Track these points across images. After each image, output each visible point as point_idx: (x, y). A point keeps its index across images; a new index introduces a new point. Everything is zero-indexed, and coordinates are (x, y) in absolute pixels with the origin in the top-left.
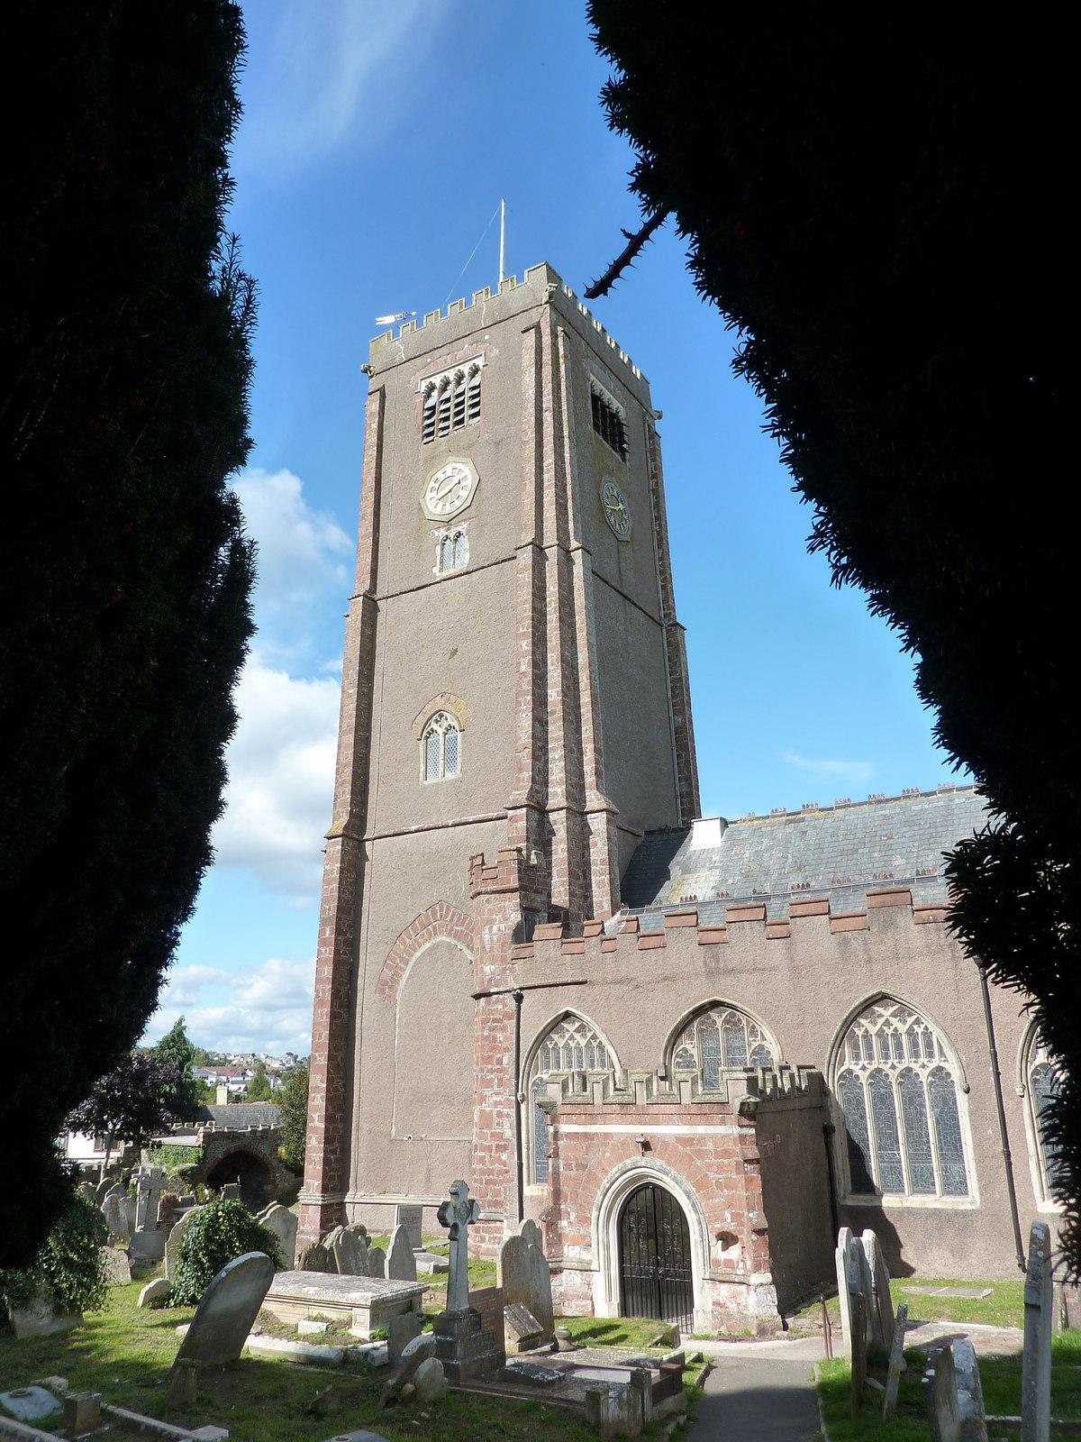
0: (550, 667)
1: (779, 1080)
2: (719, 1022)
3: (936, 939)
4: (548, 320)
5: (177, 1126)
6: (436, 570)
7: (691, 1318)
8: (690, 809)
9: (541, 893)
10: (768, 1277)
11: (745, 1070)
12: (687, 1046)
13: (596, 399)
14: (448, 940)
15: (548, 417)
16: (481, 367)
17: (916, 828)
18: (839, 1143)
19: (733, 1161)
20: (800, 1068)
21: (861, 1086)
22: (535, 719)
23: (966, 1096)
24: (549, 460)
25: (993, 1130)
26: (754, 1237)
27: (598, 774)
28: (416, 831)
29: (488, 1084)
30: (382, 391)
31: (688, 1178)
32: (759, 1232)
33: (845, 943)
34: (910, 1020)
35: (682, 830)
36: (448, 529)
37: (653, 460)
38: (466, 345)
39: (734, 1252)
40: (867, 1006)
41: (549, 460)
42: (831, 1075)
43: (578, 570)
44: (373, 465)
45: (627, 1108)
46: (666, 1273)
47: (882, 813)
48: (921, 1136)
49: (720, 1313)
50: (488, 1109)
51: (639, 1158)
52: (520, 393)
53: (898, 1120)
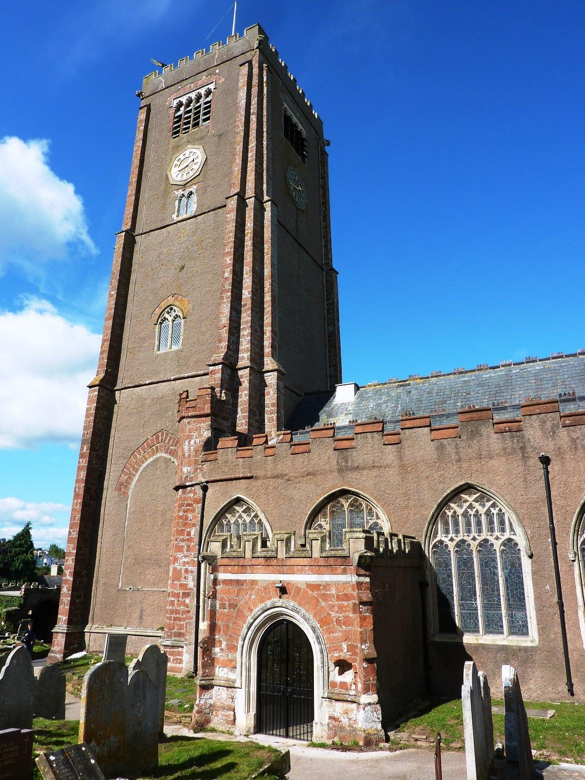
0: (245, 276)
1: (390, 544)
2: (346, 505)
3: (510, 444)
4: (258, 59)
5: (12, 585)
6: (174, 216)
7: (312, 726)
8: (336, 378)
9: (228, 420)
10: (374, 698)
11: (364, 531)
12: (322, 523)
13: (287, 119)
14: (165, 455)
15: (253, 118)
16: (212, 90)
17: (487, 387)
18: (431, 592)
19: (351, 603)
20: (405, 537)
21: (449, 554)
22: (232, 308)
23: (530, 561)
24: (252, 144)
25: (550, 586)
26: (365, 665)
27: (273, 346)
28: (150, 384)
29: (179, 549)
30: (149, 107)
31: (315, 616)
32: (368, 660)
33: (441, 448)
34: (488, 504)
35: (329, 392)
36: (184, 190)
37: (323, 168)
38: (204, 77)
39: (348, 676)
40: (455, 495)
41: (252, 144)
42: (427, 544)
43: (268, 215)
44: (139, 152)
45: (270, 561)
46: (294, 692)
47: (462, 379)
48: (493, 591)
49: (334, 726)
50: (178, 567)
51: (277, 599)
52: (235, 102)
53: (477, 579)
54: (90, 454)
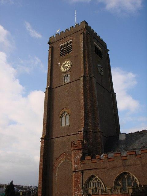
13: (96, 47)
54: (43, 160)
